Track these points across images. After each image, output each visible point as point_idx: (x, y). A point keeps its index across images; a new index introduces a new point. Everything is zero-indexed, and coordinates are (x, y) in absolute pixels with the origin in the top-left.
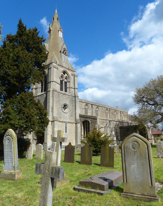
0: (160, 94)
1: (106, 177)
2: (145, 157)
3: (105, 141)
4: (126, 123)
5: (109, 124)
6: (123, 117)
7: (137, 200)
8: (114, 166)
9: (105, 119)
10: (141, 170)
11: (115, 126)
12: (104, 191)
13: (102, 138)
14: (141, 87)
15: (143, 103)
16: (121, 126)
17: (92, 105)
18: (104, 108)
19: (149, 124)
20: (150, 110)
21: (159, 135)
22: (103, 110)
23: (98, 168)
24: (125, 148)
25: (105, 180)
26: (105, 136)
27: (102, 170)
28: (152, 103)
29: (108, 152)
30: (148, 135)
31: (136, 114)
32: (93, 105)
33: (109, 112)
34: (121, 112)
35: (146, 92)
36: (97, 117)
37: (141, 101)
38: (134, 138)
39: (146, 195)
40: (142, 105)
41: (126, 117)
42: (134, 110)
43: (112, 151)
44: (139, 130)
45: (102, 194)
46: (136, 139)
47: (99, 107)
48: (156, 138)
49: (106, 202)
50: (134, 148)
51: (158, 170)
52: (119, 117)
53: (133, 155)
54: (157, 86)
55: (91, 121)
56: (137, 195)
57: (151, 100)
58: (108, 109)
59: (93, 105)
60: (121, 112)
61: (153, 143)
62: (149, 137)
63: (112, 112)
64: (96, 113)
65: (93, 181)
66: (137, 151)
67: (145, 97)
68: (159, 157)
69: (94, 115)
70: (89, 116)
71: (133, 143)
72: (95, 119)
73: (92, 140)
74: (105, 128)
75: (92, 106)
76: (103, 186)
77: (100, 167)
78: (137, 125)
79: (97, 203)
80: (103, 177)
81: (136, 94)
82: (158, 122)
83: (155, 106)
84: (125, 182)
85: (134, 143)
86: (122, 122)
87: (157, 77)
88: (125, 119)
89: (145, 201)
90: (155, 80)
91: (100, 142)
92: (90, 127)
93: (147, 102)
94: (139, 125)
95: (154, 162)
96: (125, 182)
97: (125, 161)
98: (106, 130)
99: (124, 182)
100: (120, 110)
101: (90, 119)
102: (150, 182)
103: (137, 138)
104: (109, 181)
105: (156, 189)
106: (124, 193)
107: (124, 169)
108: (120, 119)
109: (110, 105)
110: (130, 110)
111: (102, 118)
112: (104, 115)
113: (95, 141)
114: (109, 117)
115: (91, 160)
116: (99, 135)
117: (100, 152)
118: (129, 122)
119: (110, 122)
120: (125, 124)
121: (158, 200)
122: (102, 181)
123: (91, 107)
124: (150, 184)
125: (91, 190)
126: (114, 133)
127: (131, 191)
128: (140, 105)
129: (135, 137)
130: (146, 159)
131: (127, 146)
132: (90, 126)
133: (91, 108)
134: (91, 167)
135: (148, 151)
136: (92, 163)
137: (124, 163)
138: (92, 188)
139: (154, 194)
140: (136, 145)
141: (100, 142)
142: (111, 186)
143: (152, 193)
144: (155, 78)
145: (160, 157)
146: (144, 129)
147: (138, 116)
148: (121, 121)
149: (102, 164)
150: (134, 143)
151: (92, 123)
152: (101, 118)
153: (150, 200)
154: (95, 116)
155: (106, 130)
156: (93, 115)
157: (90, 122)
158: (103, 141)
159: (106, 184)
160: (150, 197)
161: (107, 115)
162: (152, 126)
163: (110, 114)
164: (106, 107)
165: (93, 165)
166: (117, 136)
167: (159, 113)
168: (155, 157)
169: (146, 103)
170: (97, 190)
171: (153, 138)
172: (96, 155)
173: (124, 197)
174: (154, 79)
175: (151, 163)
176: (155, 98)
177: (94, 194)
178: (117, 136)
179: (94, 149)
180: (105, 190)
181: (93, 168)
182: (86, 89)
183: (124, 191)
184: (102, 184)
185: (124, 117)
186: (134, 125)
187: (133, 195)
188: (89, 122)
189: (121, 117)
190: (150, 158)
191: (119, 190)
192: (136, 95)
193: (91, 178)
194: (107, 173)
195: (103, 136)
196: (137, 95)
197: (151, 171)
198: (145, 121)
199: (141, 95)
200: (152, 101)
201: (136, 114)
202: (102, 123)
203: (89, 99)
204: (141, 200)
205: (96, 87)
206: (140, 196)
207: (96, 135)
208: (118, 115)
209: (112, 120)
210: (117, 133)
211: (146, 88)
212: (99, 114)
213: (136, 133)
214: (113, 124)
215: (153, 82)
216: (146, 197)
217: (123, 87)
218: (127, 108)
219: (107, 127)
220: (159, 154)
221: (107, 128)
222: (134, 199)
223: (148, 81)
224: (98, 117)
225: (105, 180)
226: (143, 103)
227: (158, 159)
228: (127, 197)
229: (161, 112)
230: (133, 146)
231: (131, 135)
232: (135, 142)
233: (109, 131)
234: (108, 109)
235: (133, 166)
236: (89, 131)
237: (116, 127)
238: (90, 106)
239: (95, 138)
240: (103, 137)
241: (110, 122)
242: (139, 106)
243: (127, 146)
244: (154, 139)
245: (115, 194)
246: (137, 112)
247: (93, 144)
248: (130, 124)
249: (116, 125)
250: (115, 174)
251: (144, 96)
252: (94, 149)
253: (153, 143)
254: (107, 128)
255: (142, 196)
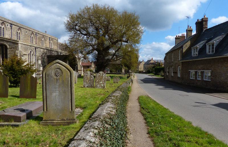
0: (93, 24)
1: (24, 108)
2: (67, 85)
3: (27, 70)
4: (55, 51)
5: (34, 52)
6: (53, 44)
7: (56, 125)
8: (37, 97)
9: (30, 45)
10: (62, 97)
11: (42, 54)
12: (21, 122)
13: (23, 67)
14: (75, 12)
15: (75, 31)
16: (50, 54)
17: (11, 24)
18: (28, 32)
19: (80, 55)
20: (82, 40)
21: (88, 67)
22: (27, 33)
23: (16, 100)
24: (46, 76)
25: (23, 111)
26: (28, 65)
27: (21, 102)
28: (84, 32)
29: (29, 82)
30: (77, 66)
31: (67, 42)
32: (14, 25)
33: (35, 37)
34: (51, 39)
35: (79, 20)
36: (18, 41)
37: (73, 28)
38: (57, 65)
39: (65, 119)
40: (75, 33)
41: (56, 46)
42: (65, 39)
43: (34, 81)
44: (69, 60)
45: (17, 126)
46: (60, 66)
47: (22, 29)
48: (85, 70)
49: (22, 133)
50: (56, 76)
51: (81, 98)
52: (47, 45)
53: (55, 83)
54: (91, 16)
55: (9, 45)
56: (56, 121)
57: (84, 29)
58: (35, 33)
59: (14, 25)
60: (51, 39)
61: (82, 74)
62: (79, 69)
63: (39, 38)
64: (17, 36)
65: (6, 114)
66: (59, 78)
67: (78, 25)
68: (84, 87)
69: (15, 38)
70: (6, 39)
71: (56, 70)
72: (15, 43)
73: (10, 68)
74: (30, 56)
75: (11, 27)
76: (20, 118)
77: (19, 99)
78: (67, 54)
79: (10, 135)
80: (19, 108)
81: (69, 20)
82: (88, 53)
83: (88, 36)
84: (45, 110)
85: (57, 70)
86: (51, 50)
87: (92, 5)
88: (55, 47)
89: (64, 125)
90: (90, 8)
91: (21, 71)
92: (8, 53)
93: (79, 31)
94: (70, 54)
95: (75, 89)
96: (45, 110)
97: (46, 89)
98: (30, 58)
99: (44, 110)
100: (49, 36)
101: (9, 43)
102: (70, 107)
103: (60, 65)
104: (27, 112)
105: (75, 113)
106: (43, 121)
107: (45, 97)
108: (48, 46)
109: (38, 28)
110: (62, 37)
111: (25, 43)
112: (28, 39)
113: (14, 70)
114: (35, 43)
115: (7, 91)
116: (19, 63)
117: (19, 82)
118: (59, 51)
119: (35, 49)
120: (53, 52)
121: (76, 122)
122: (19, 112)
123: (9, 26)
124: (70, 110)
125: (3, 123)
126: (40, 62)
127: (51, 118)
128: (72, 33)
129: (58, 64)
130: (68, 86)
131: (49, 74)
132: (8, 52)
133: (10, 29)
134: (7, 99)
135: (71, 76)
136: (9, 94)
137: (45, 91)
138: (5, 122)
139: (73, 118)
140: (59, 72)
141: (21, 71)
142: (30, 116)
143: (71, 117)
144: (90, 5)
145: (86, 86)
146: (74, 59)
147: (69, 46)
148: (50, 49)
149: (22, 96)
150: (57, 70)
151: (11, 48)
152: (24, 43)
153: (69, 124)
154: (16, 39)
155: (30, 58)
156: (13, 38)
157: (8, 47)
158: (24, 70)
159: (23, 115)
160: (69, 121)
161: (32, 41)
162: (82, 57)
163: (37, 40)
164: (31, 30)
165: (9, 97)
166: (44, 65)
167: (90, 44)
168: (82, 87)
169: (78, 32)
170: (11, 122)
171: (82, 69)
172: (15, 87)
173: (43, 125)
174: (89, 7)
175: (72, 90)
176: (88, 28)
177: (7, 127)
178: (44, 65)
179: (12, 79)
180: (22, 121)
181: (9, 100)
182: (4, 2)
183: (44, 119)
184: (18, 115)
185: (54, 45)
186: (64, 55)
187: (52, 121)
188: (6, 46)
189: (50, 44)
190: (72, 86)
191: (39, 119)
192: (68, 21)
193: (3, 111)
194: (27, 104)
195: (25, 64)
196: (70, 21)
197: (72, 98)
198: (76, 52)
199: (74, 22)
200: (85, 30)
201: (67, 42)
202: (26, 50)
203: (9, 17)
204: (60, 125)
205: (19, 2)
206: (60, 121)
207: (15, 63)
208: (47, 42)
209: (38, 46)
210: (45, 63)
211: (80, 15)
212: (22, 37)
213: (66, 62)
214: (40, 51)
215: (88, 9)
216: (66, 121)
217: (55, 10)
218: (59, 35)
219: (32, 55)
220: (85, 84)
221: (32, 56)
222: (53, 125)
223: (83, 8)
224: (19, 42)
225: (23, 111)
226: (75, 31)
227: (84, 88)
228: (46, 124)
229: (92, 44)
230: (55, 73)
231: (55, 62)
232: (58, 70)
233: (34, 60)
234: (34, 33)
235: (54, 94)
236: (6, 58)
237: (44, 56)
238: (7, 25)
239: (14, 66)
240: (25, 65)
241: (35, 49)
242: (70, 35)
243: (49, 74)
244: (83, 70)
245: (33, 123)
246: (69, 40)
247: (11, 73)
248: (59, 53)
249: (43, 54)
250: (34, 105)
251: (77, 24)
252: (12, 79)
253: (82, 74)
254: (32, 56)
255: (62, 121)
